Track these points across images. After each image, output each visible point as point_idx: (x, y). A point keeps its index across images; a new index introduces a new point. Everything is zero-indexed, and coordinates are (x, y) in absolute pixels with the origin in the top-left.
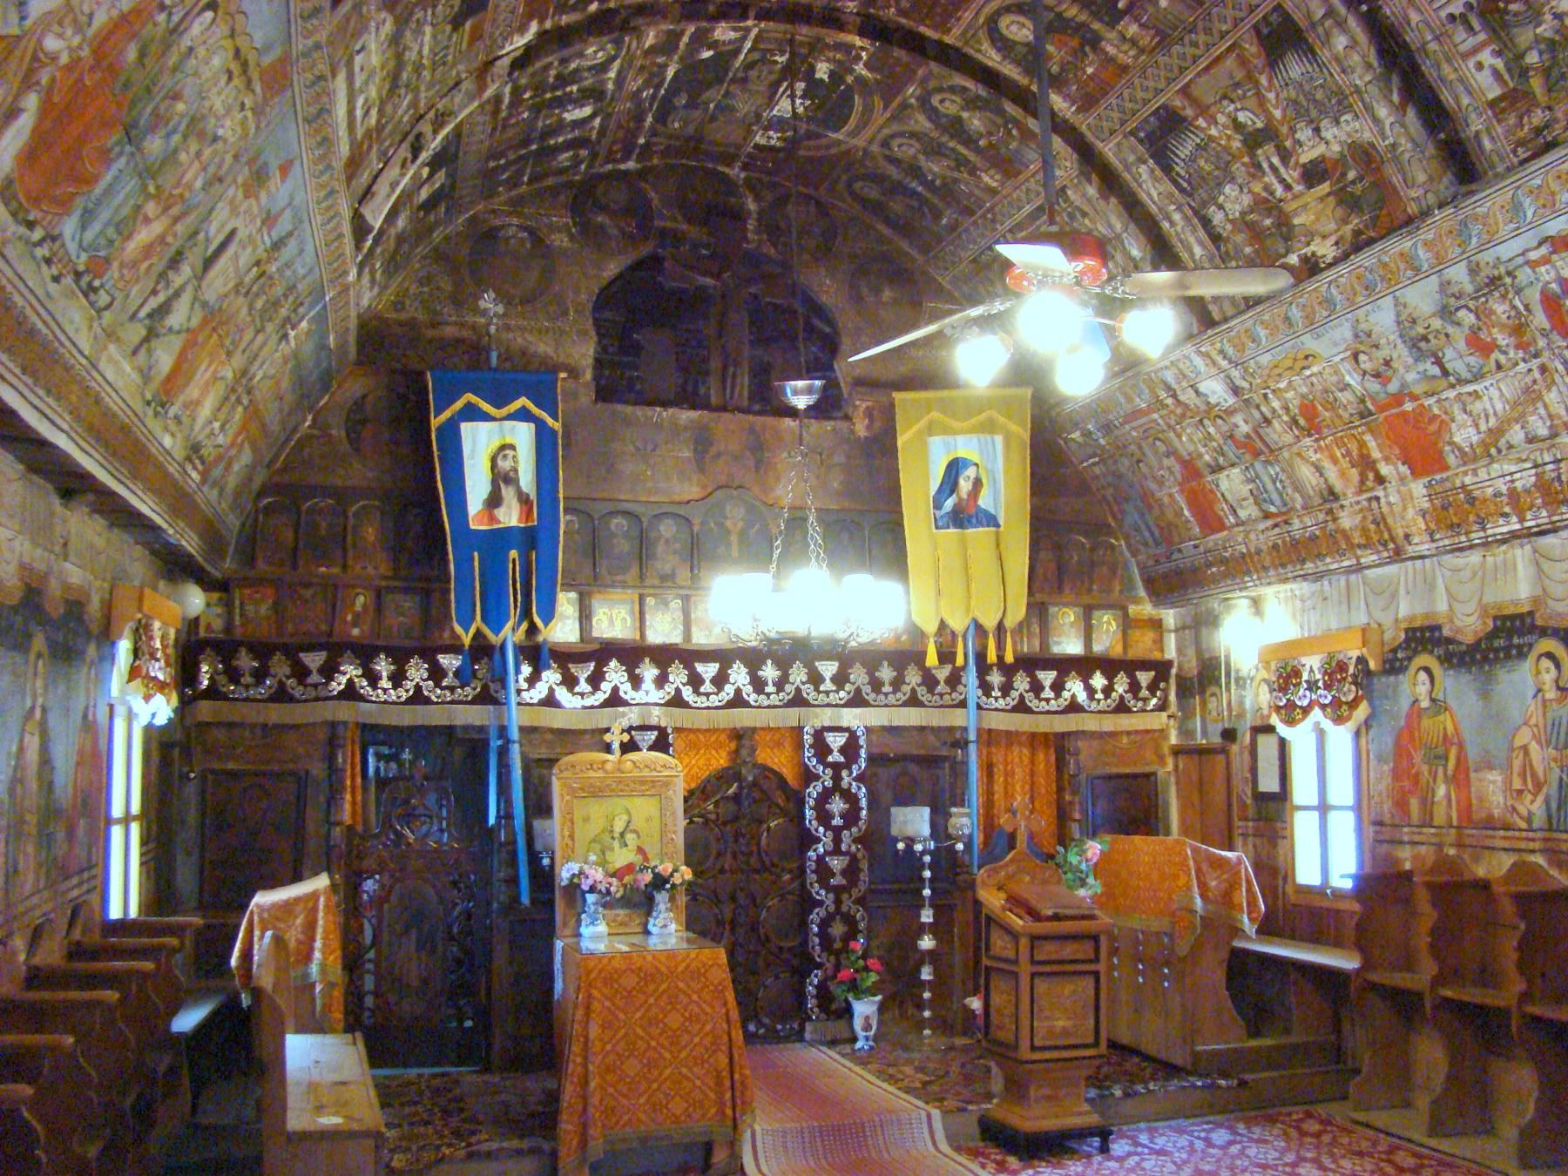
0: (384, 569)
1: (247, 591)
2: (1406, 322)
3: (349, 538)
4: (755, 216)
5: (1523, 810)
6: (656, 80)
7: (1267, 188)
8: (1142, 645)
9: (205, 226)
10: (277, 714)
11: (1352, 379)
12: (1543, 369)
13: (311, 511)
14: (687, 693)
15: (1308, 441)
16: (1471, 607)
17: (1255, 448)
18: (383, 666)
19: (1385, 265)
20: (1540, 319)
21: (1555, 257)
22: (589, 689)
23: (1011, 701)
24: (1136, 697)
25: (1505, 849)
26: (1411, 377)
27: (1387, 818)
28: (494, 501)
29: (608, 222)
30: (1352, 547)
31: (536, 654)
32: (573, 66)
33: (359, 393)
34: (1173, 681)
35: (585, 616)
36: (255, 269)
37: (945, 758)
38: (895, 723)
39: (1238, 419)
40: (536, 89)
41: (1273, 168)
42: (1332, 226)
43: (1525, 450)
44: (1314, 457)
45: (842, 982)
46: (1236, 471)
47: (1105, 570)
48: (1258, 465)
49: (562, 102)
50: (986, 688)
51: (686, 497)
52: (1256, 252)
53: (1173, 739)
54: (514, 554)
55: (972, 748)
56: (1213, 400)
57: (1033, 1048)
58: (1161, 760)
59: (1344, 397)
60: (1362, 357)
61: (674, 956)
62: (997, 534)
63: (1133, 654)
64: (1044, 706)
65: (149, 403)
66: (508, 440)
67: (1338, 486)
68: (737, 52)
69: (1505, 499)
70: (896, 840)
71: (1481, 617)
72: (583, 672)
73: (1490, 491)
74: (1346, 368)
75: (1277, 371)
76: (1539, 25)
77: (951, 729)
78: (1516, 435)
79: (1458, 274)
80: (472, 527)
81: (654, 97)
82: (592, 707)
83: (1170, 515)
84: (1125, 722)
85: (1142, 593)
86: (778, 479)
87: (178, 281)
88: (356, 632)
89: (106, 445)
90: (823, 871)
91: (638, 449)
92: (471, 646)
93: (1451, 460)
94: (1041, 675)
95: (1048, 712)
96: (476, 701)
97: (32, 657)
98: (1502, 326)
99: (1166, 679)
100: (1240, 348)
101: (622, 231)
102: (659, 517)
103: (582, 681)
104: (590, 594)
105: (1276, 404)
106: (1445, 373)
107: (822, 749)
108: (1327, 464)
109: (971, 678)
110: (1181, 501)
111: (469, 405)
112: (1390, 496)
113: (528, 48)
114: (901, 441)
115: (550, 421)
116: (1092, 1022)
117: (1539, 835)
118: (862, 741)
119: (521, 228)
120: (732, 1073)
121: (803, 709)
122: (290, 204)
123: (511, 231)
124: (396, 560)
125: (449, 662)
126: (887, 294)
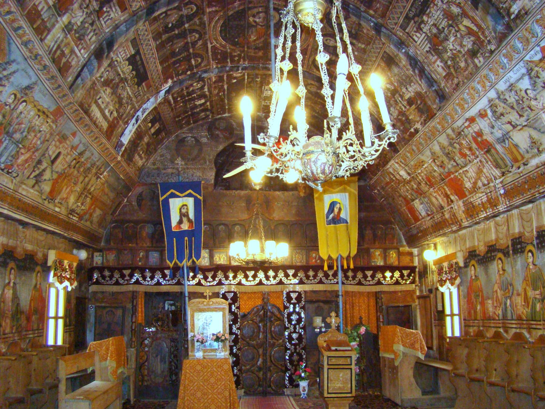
0: (149, 244)
1: (107, 252)
2: (443, 148)
3: (138, 236)
5: (497, 313)
6: (222, 90)
7: (400, 107)
8: (406, 261)
9: (47, 152)
10: (115, 289)
11: (436, 168)
12: (481, 161)
13: (127, 227)
14: (203, 282)
15: (431, 190)
16: (482, 244)
17: (420, 193)
18: (148, 274)
19: (430, 131)
20: (474, 146)
21: (471, 125)
22: (212, 280)
23: (356, 282)
24: (403, 279)
25: (493, 327)
26: (450, 166)
27: (467, 318)
28: (180, 222)
29: (219, 133)
30: (450, 224)
31: (194, 269)
32: (191, 89)
33: (140, 192)
34: (417, 273)
35: (211, 257)
36: (74, 161)
37: (333, 301)
38: (315, 289)
39: (412, 183)
40: (181, 97)
41: (400, 102)
42: (418, 119)
43: (482, 189)
44: (435, 195)
45: (296, 375)
46: (417, 200)
47: (390, 236)
48: (422, 198)
49: (194, 99)
50: (347, 277)
51: (243, 218)
52: (403, 128)
53: (418, 293)
54: (186, 238)
55: (340, 297)
56: (404, 177)
57: (328, 393)
58: (414, 301)
59: (436, 174)
60: (436, 161)
61: (213, 361)
63: (402, 264)
64: (368, 283)
65: (45, 200)
66: (185, 203)
67: (443, 204)
68: (244, 79)
69: (481, 206)
70: (315, 328)
71: (485, 246)
72: (210, 275)
73: (477, 203)
74: (433, 164)
75: (416, 167)
76: (447, 53)
77: (333, 291)
78: (480, 184)
79: (449, 131)
80: (173, 230)
81: (224, 94)
82: (213, 285)
83: (406, 216)
84: (398, 288)
85: (405, 243)
86: (274, 211)
87: (42, 167)
88: (140, 263)
89: (27, 211)
90: (290, 338)
92: (173, 267)
93: (467, 193)
94: (367, 272)
95: (370, 285)
96: (176, 284)
97: (9, 269)
98: (466, 148)
99: (414, 272)
100: (405, 160)
102: (236, 224)
103: (210, 277)
104: (213, 250)
105: (420, 178)
106: (458, 165)
107: (289, 298)
108: (438, 197)
109: (340, 274)
110: (406, 211)
112: (455, 206)
113: (170, 87)
115: (199, 197)
116: (350, 385)
117: (501, 322)
118: (303, 296)
120: (230, 397)
121: (282, 286)
122: (80, 143)
123: (189, 138)
124: (152, 242)
125: (167, 272)
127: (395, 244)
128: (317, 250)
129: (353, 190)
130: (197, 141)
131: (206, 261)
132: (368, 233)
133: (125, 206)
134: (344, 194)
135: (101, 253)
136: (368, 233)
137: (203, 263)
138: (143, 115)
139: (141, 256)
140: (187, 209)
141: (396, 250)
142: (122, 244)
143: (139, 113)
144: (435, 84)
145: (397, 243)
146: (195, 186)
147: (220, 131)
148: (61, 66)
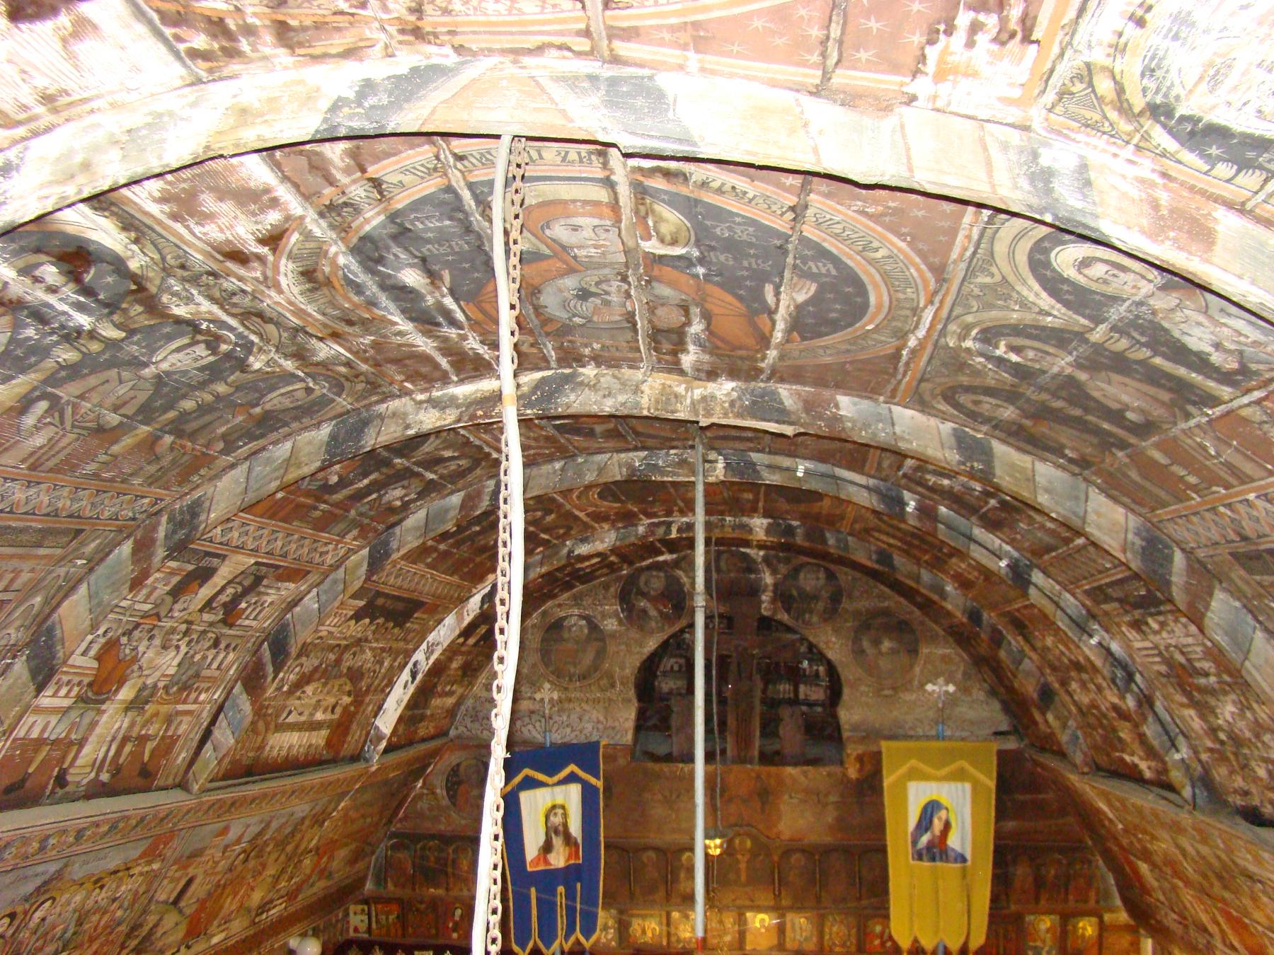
1: (380, 906)
4: (771, 588)
28: (547, 847)
29: (649, 605)
33: (454, 763)
35: (623, 927)
54: (561, 889)
62: (964, 869)
80: (529, 869)
88: (455, 935)
91: (665, 797)
101: (661, 613)
111: (527, 778)
114: (887, 782)
115: (593, 780)
119: (581, 617)
123: (573, 620)
126: (887, 645)
127: (1092, 903)
128: (887, 917)
129: (982, 777)
130: (593, 626)
131: (610, 937)
132: (1022, 873)
133: (420, 797)
134: (959, 785)
135: (366, 908)
136: (1022, 873)
137: (603, 940)
138: (427, 659)
139: (457, 918)
140: (565, 815)
141: (1094, 920)
142: (414, 889)
143: (419, 656)
144: (1181, 741)
145: (1097, 902)
146: (584, 754)
147: (653, 600)
148: (146, 758)
